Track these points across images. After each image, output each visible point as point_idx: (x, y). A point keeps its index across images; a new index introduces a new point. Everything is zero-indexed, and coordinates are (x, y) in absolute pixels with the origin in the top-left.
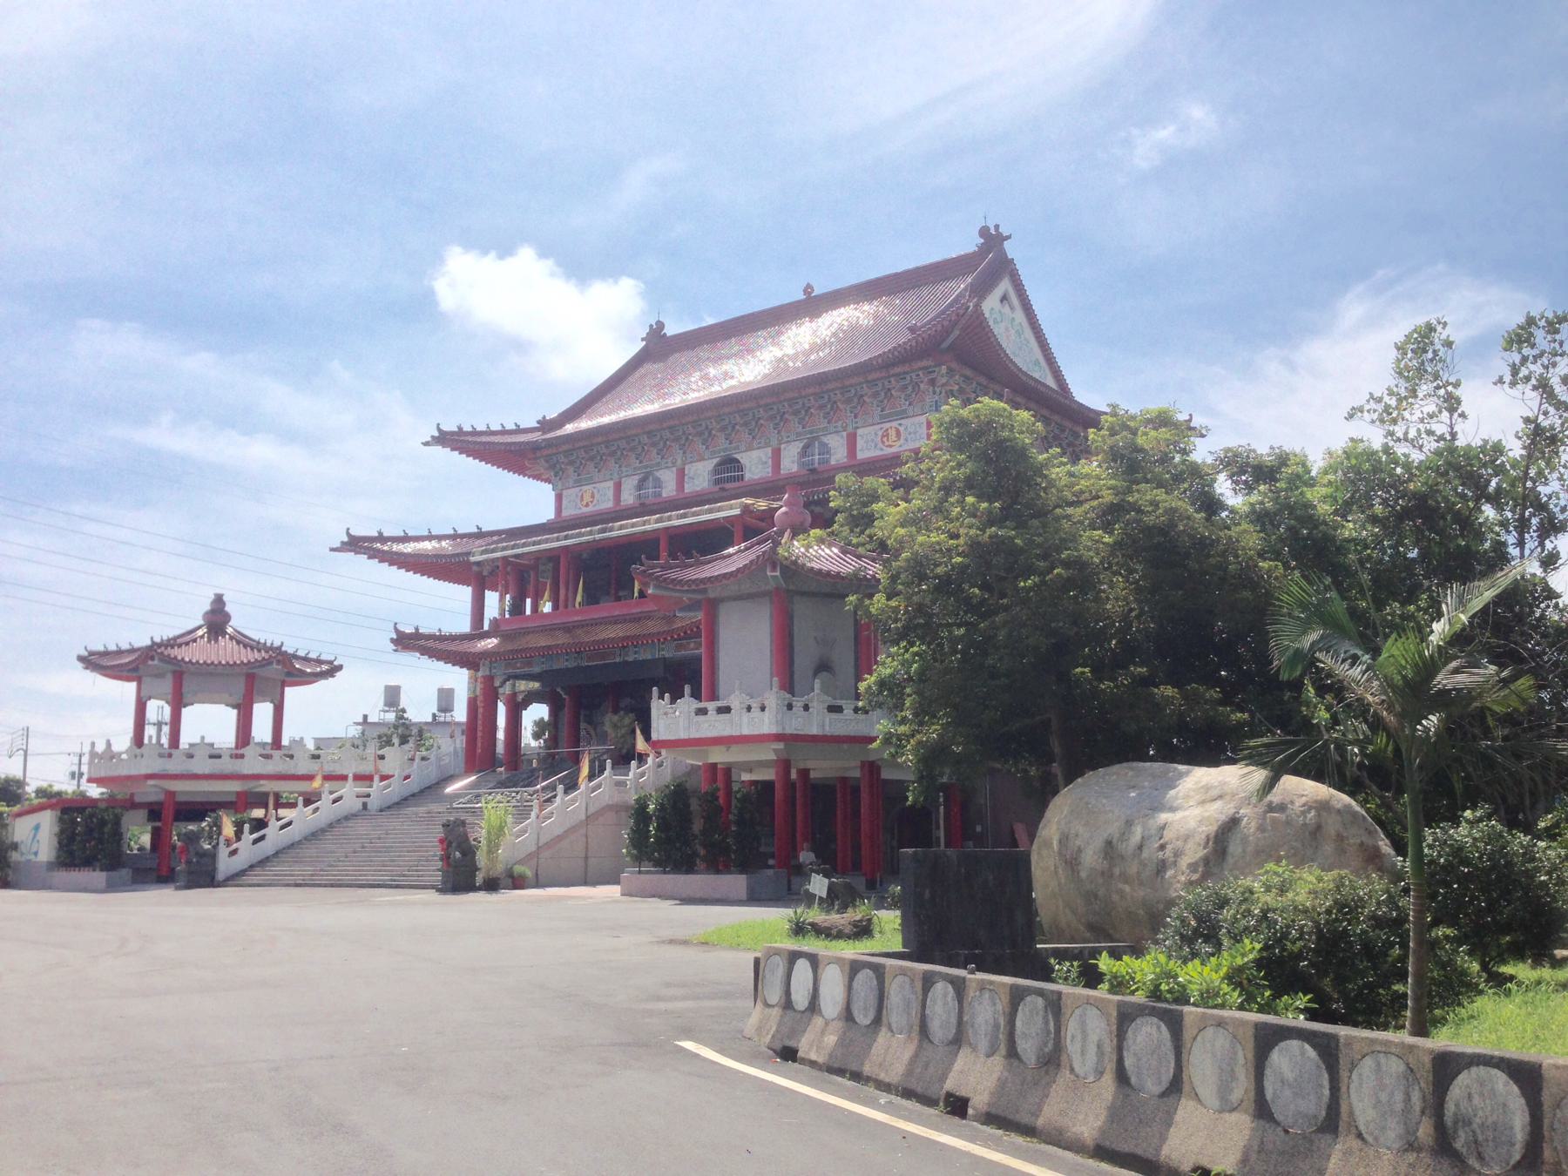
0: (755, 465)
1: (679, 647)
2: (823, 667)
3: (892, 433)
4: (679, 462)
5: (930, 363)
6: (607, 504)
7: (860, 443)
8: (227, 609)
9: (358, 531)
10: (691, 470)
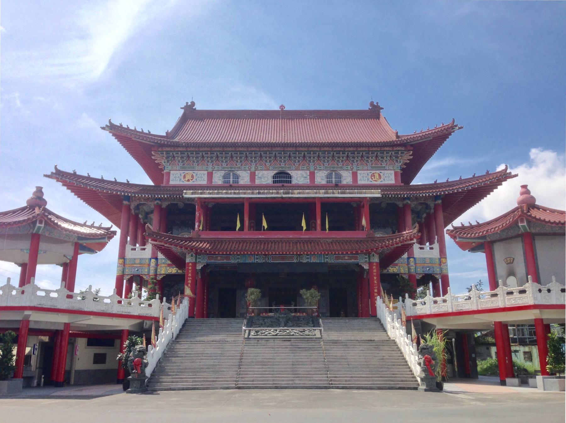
0: (299, 176)
1: (337, 258)
2: (511, 273)
3: (377, 176)
4: (253, 169)
5: (403, 149)
6: (203, 181)
7: (359, 177)
8: (504, 183)
9: (61, 168)
10: (259, 173)
